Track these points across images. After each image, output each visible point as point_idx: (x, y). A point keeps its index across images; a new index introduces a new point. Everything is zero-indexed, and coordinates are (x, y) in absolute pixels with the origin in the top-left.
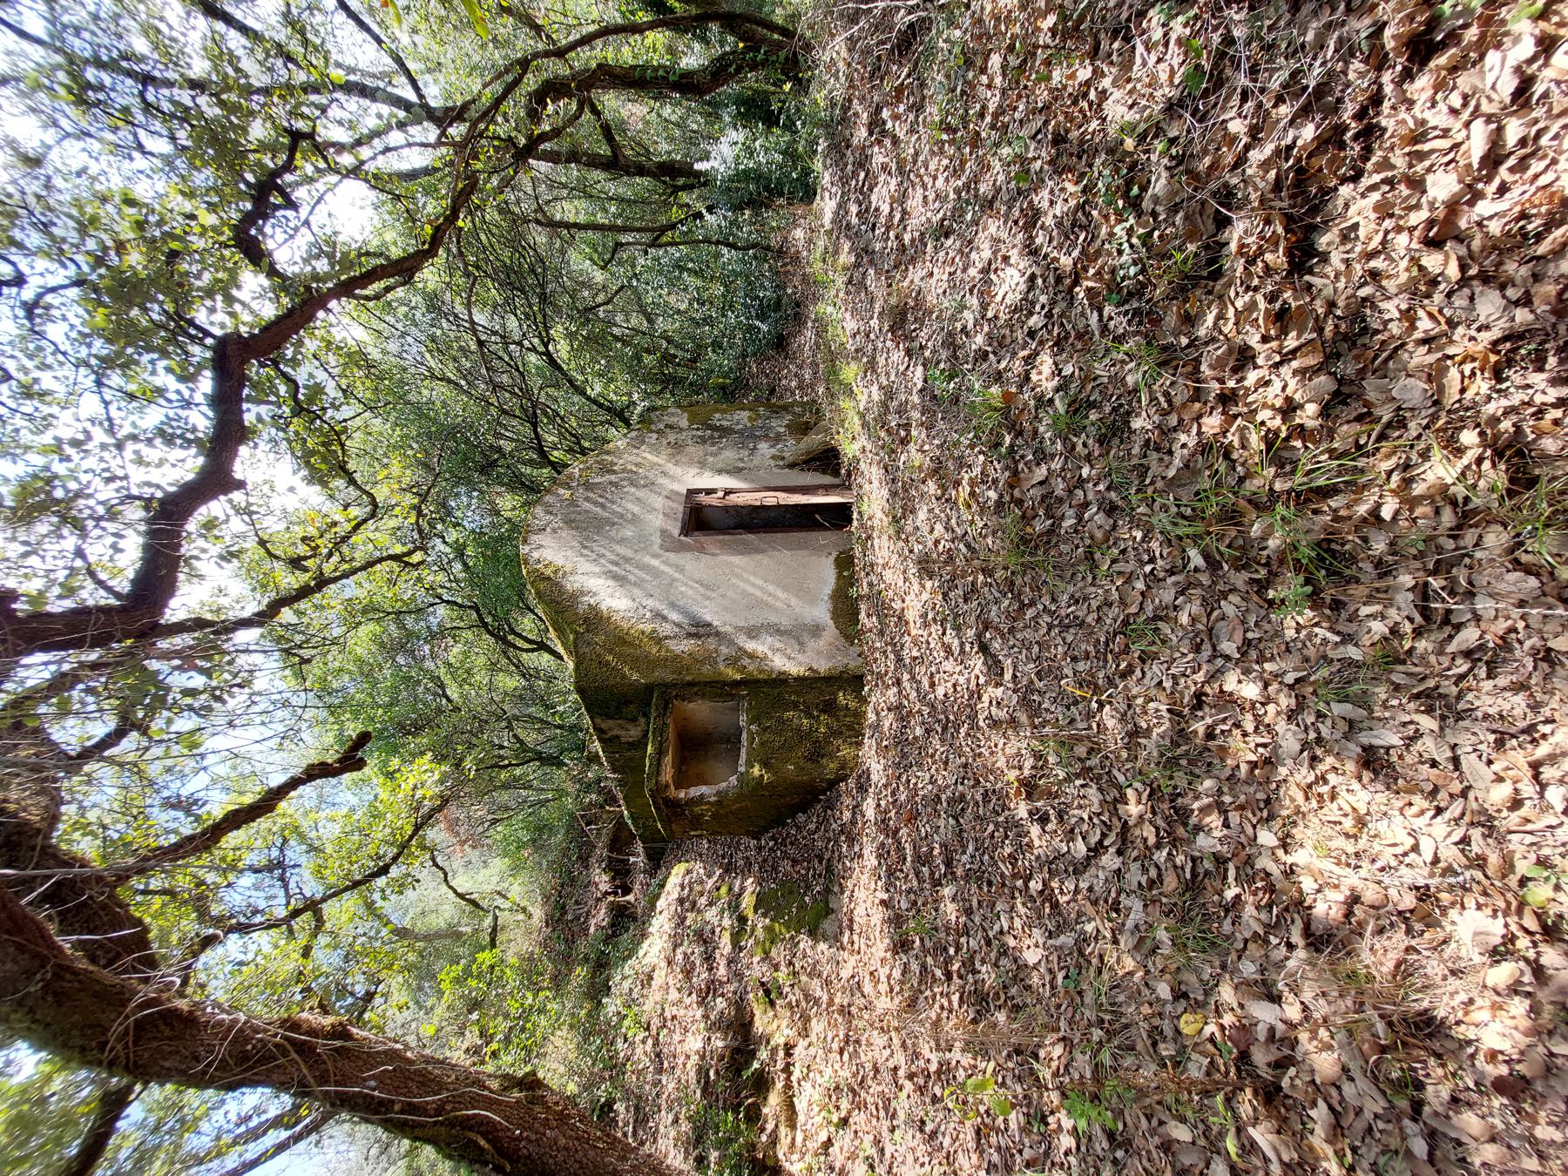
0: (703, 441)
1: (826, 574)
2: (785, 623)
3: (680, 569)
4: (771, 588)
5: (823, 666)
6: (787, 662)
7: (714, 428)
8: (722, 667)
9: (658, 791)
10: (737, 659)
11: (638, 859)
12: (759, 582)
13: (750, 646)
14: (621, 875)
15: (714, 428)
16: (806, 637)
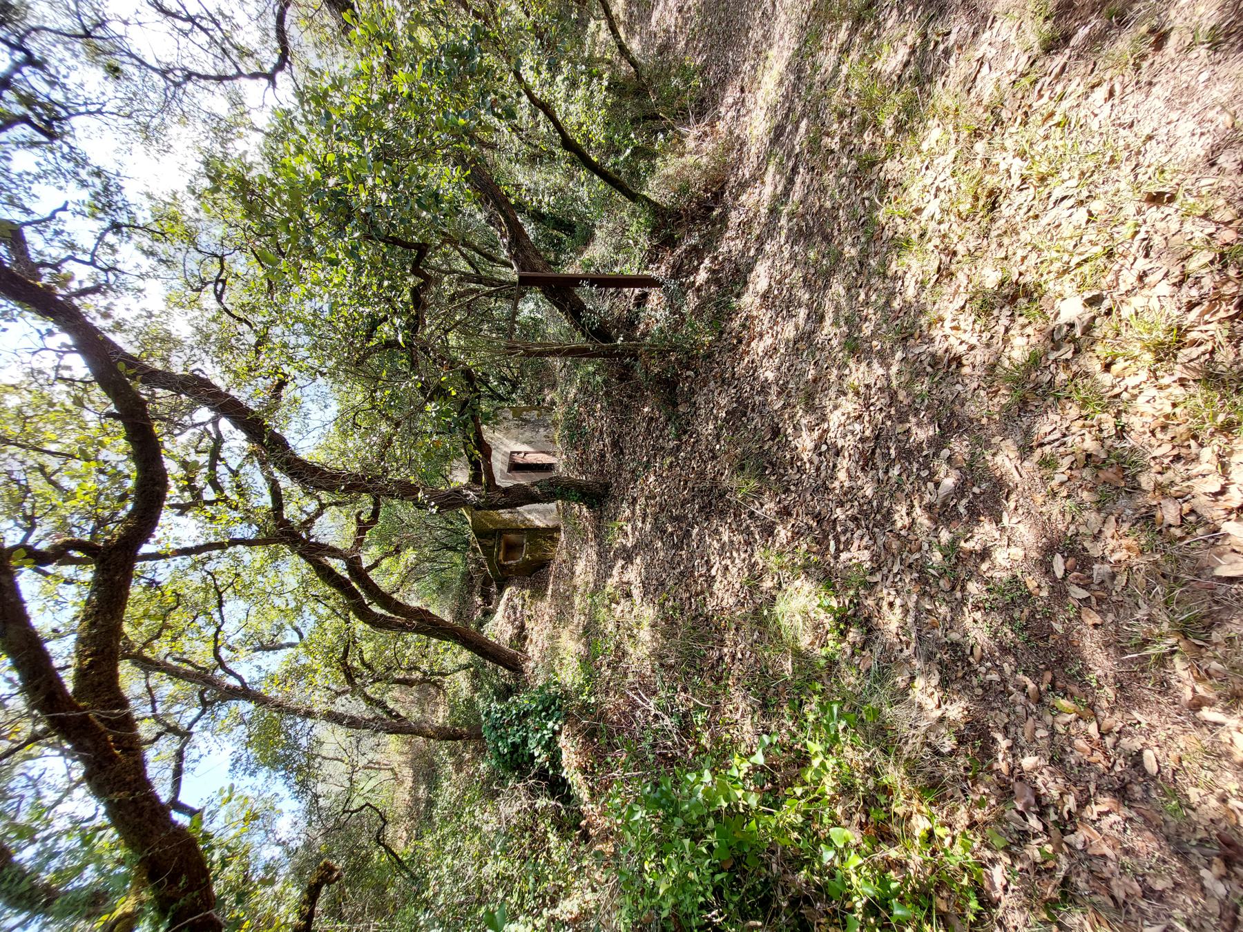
0: (518, 426)
5: (551, 524)
7: (523, 420)
9: (498, 562)
11: (494, 589)
13: (529, 516)
14: (487, 598)
15: (523, 420)
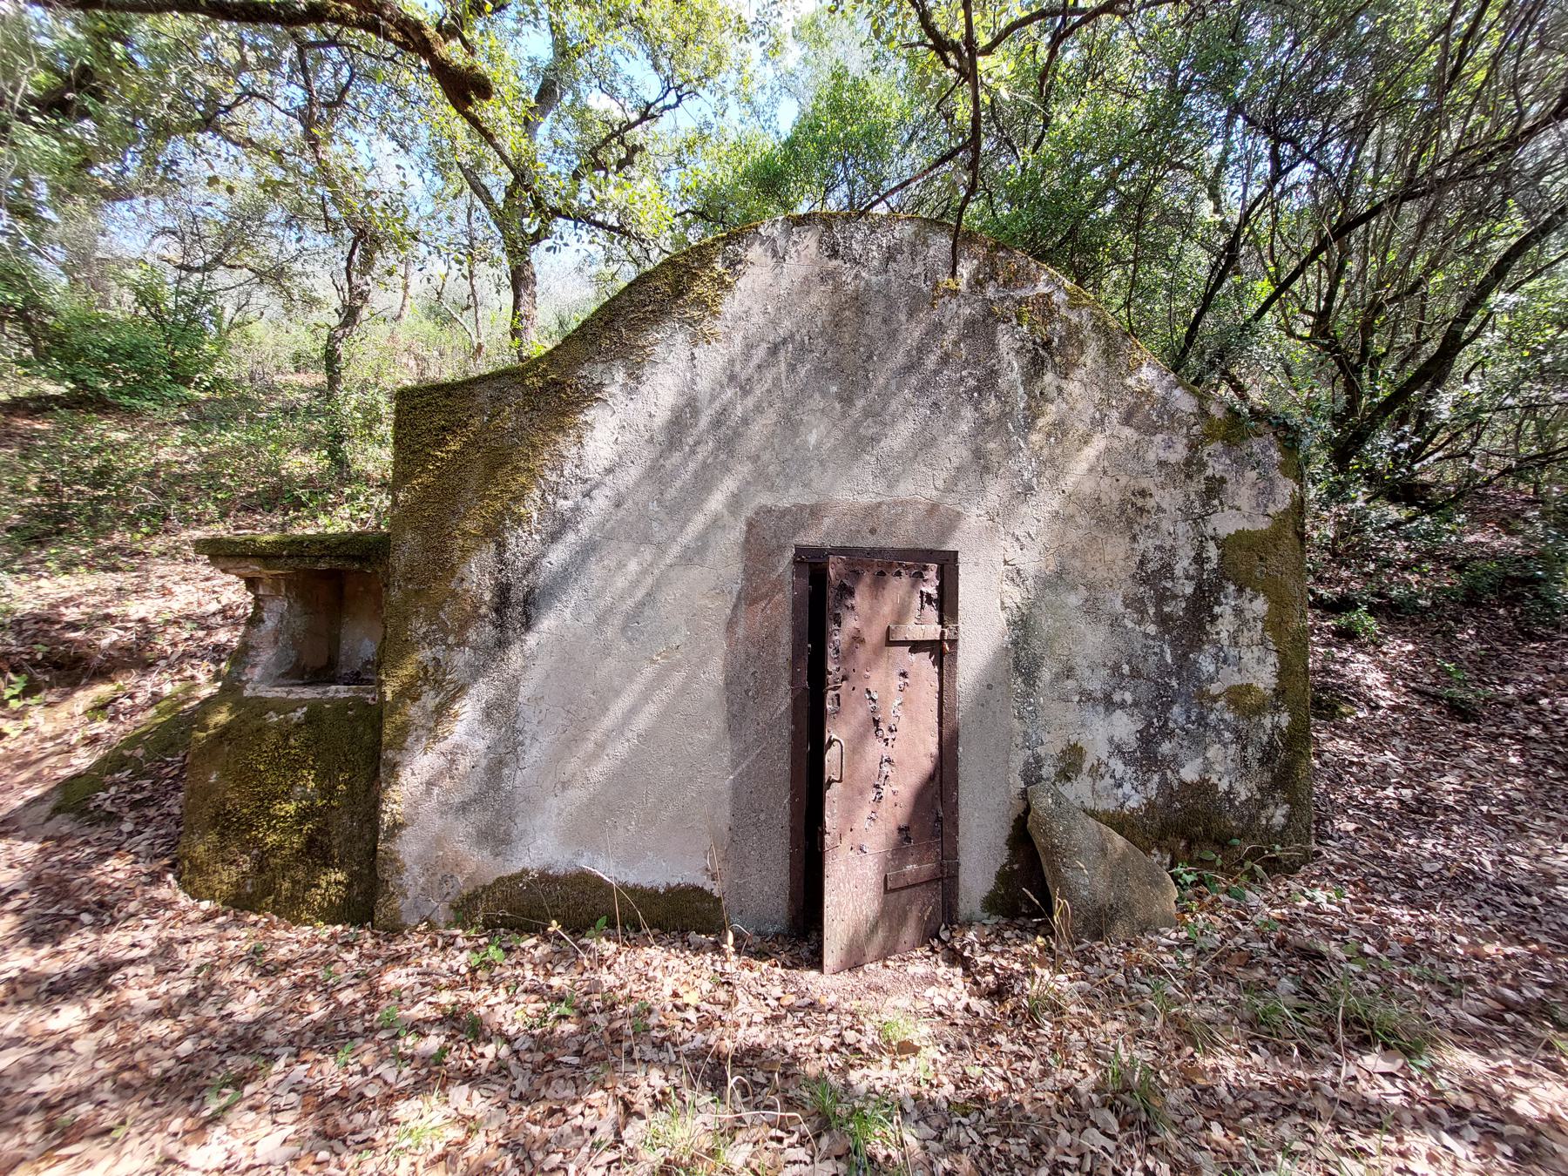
2: (519, 778)
3: (694, 555)
4: (620, 749)
6: (417, 784)
8: (425, 654)
10: (438, 685)
12: (642, 722)
13: (468, 710)
16: (477, 817)
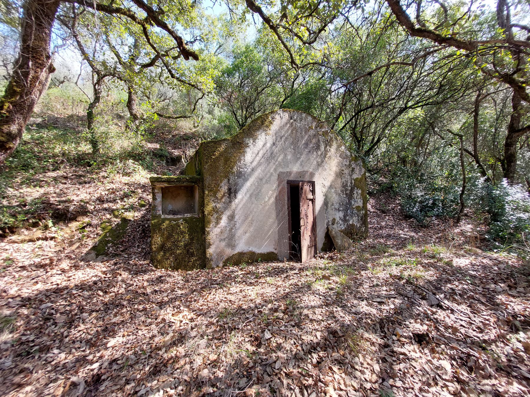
0: (344, 186)
1: (265, 247)
6: (215, 233)
7: (352, 191)
10: (217, 212)
15: (352, 191)
